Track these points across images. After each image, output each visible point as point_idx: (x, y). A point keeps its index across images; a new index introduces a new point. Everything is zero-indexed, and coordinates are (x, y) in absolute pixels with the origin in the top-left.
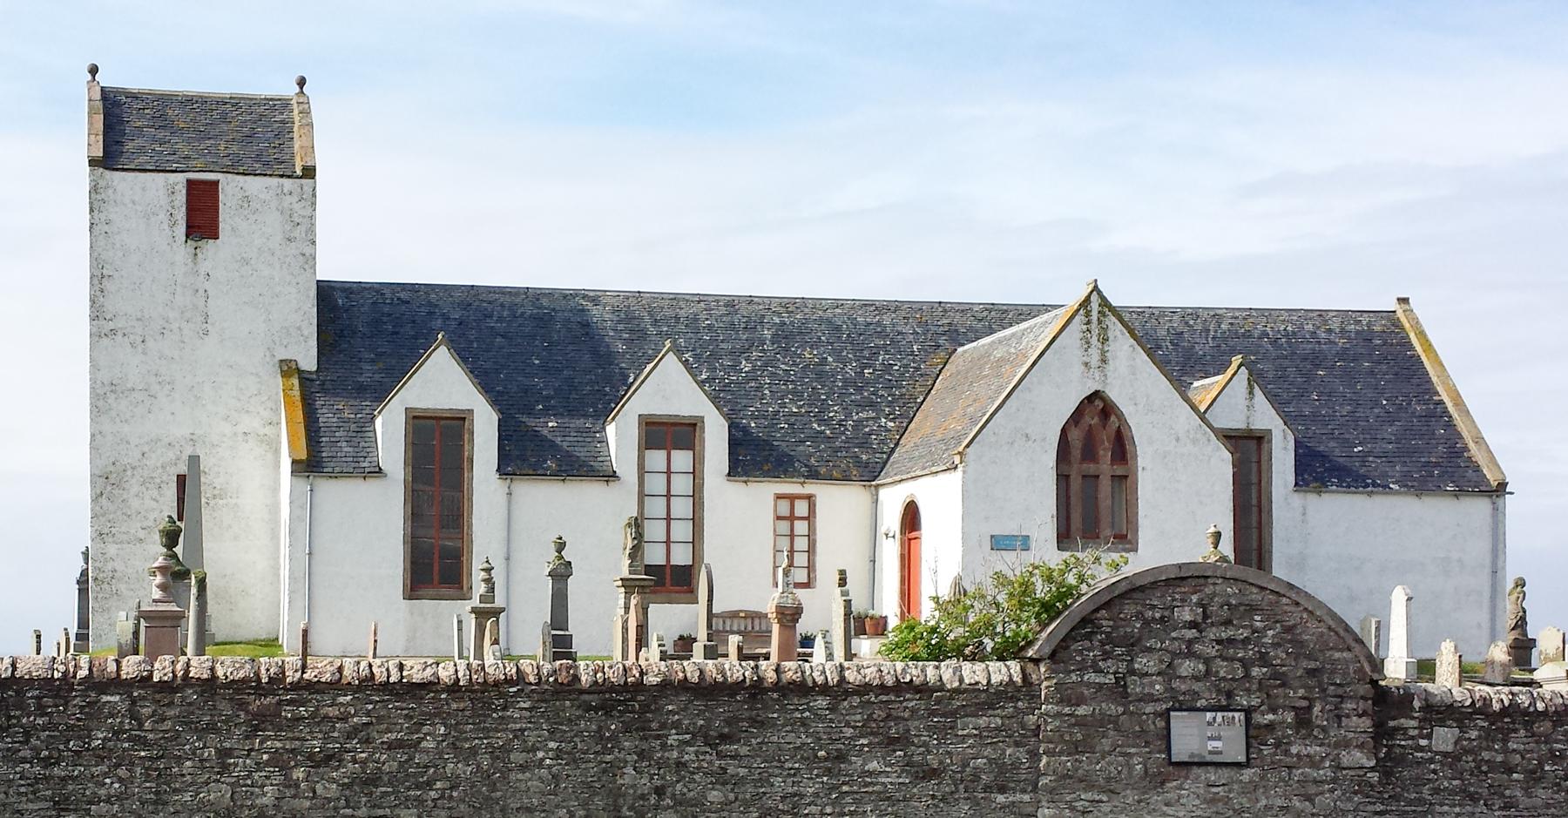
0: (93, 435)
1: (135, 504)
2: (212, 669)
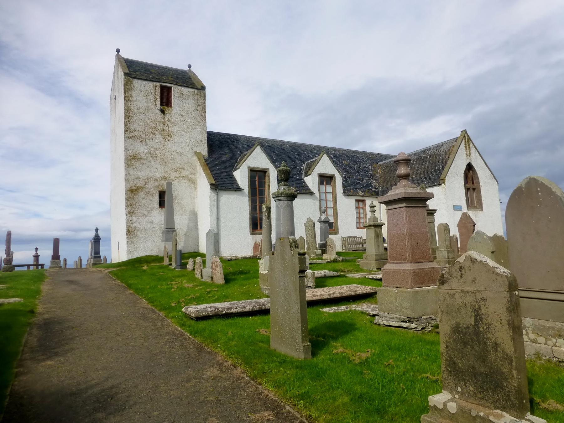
0: (126, 175)
1: (143, 201)
2: (37, 257)
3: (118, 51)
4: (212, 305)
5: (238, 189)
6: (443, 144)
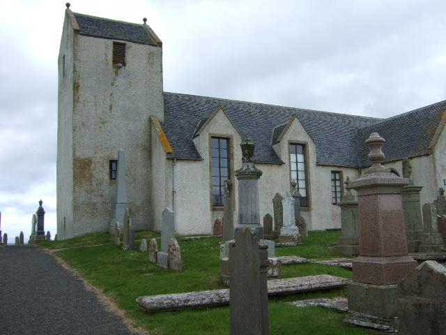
3: (68, 5)
4: (169, 296)
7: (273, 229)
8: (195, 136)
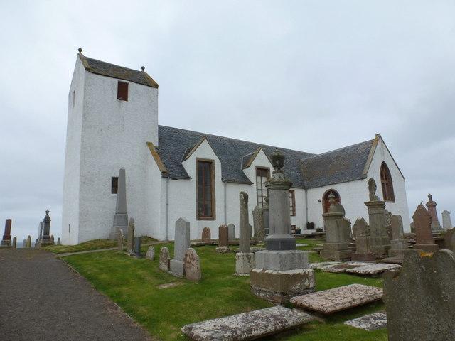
3: (80, 50)
5: (187, 177)
6: (360, 145)
7: (253, 236)
8: (184, 160)
